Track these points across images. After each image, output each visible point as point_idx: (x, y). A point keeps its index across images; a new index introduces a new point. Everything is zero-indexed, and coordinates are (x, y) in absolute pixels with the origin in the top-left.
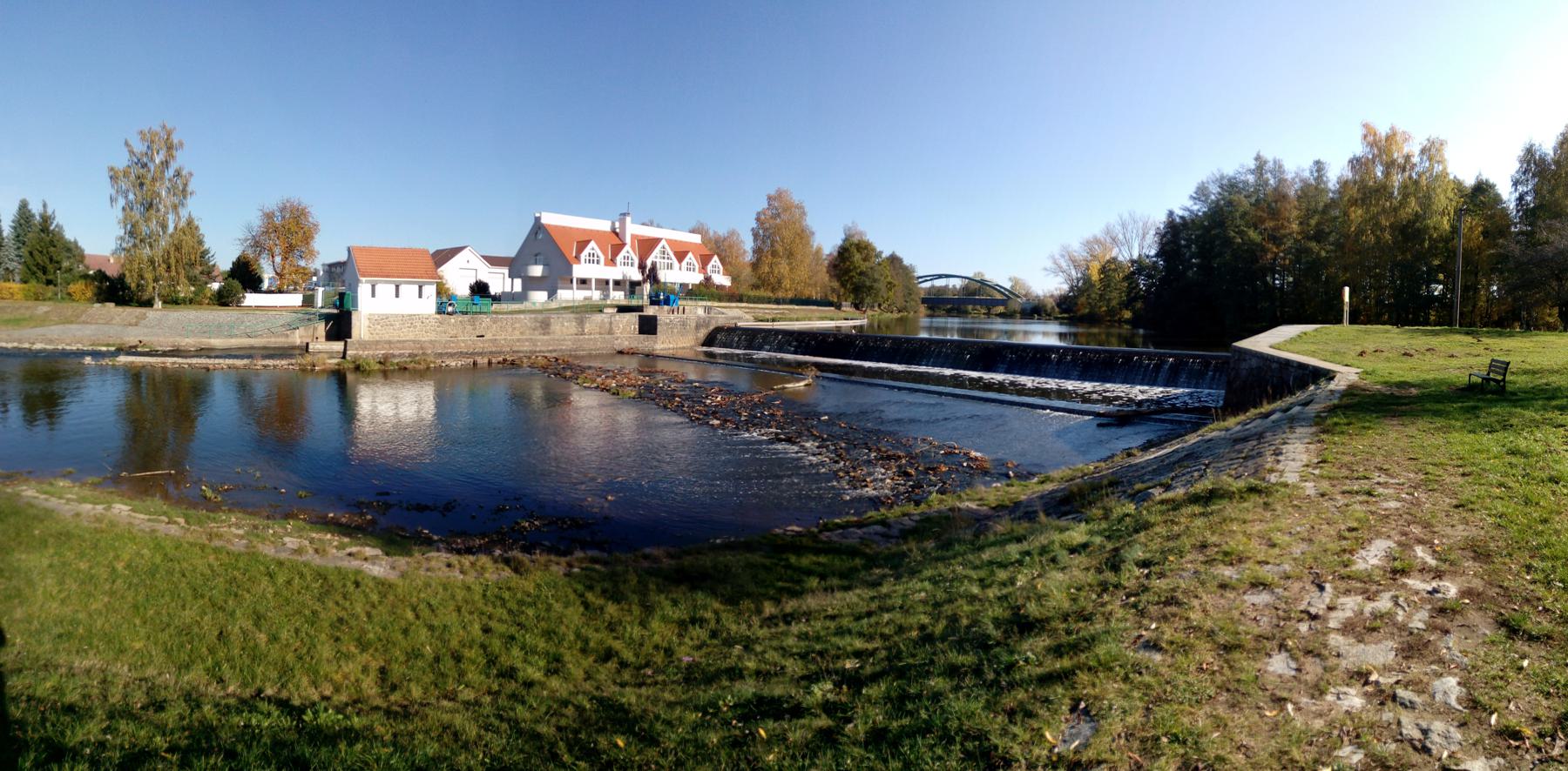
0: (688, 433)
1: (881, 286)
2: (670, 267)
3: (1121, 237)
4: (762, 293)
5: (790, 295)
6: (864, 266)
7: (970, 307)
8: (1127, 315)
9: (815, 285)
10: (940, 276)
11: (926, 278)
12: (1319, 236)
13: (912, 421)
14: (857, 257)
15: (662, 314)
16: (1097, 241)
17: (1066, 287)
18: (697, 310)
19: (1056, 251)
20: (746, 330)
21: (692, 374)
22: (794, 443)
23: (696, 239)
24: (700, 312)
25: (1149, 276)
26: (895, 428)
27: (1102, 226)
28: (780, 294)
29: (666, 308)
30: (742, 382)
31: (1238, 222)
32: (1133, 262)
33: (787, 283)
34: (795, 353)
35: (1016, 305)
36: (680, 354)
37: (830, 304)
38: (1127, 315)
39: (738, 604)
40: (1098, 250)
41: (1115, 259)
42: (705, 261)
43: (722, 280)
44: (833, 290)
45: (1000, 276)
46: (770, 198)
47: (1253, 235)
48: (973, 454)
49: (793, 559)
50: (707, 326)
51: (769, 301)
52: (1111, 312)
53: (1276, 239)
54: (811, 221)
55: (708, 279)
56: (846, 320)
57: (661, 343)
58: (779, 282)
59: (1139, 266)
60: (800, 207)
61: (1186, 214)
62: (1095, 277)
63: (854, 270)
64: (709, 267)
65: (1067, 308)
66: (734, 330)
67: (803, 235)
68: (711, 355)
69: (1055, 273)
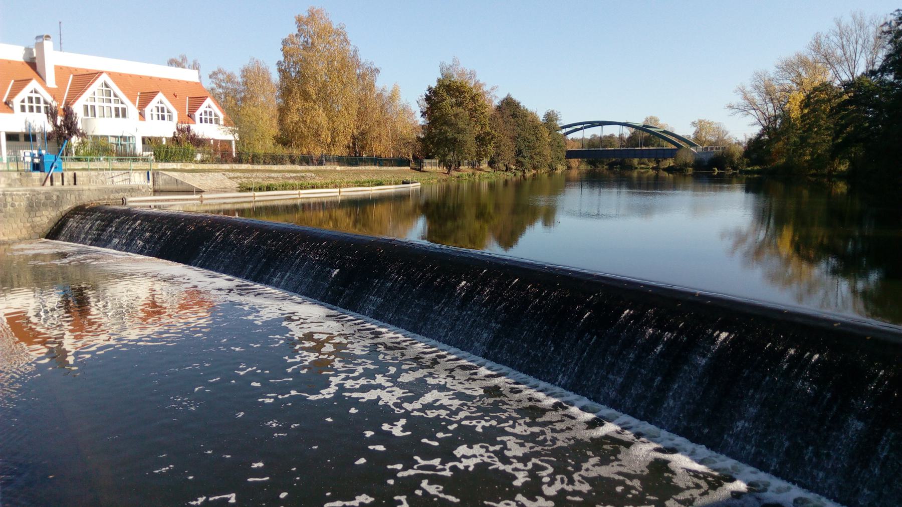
7: (636, 161)
10: (593, 124)
17: (756, 130)
35: (688, 155)
43: (213, 130)
46: (299, 20)
52: (818, 161)
62: (795, 114)
69: (745, 111)
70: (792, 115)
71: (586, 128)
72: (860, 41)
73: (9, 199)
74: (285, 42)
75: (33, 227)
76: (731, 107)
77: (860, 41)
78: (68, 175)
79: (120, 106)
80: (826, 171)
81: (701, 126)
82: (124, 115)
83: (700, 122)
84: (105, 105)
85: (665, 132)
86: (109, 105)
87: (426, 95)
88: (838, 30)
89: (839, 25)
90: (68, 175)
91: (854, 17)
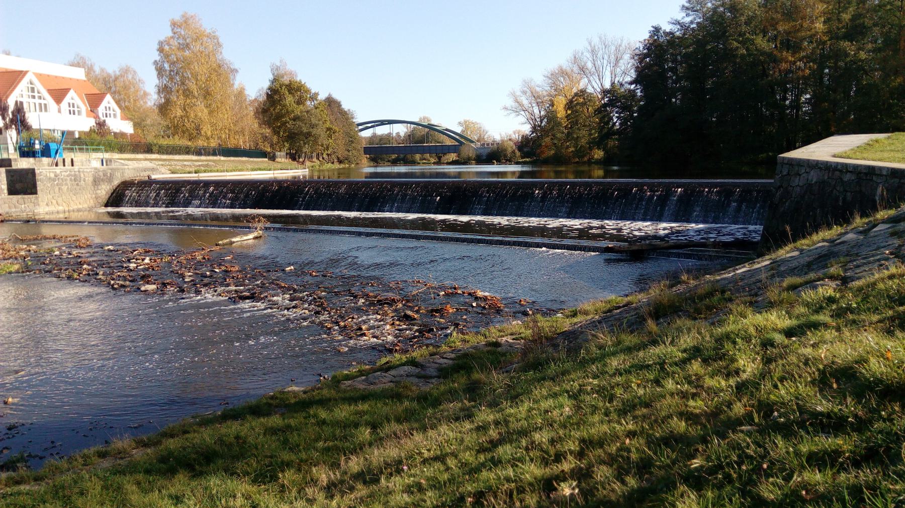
0: (92, 309)
1: (320, 131)
2: (44, 108)
3: (590, 65)
4: (178, 141)
5: (214, 144)
6: (298, 110)
7: (418, 157)
8: (599, 154)
9: (242, 132)
10: (382, 123)
11: (367, 125)
12: (855, 32)
13: (392, 265)
14: (289, 100)
15: (42, 167)
16: (563, 72)
17: (526, 129)
18: (90, 162)
19: (517, 88)
20: (164, 184)
21: (94, 235)
22: (259, 299)
23: (79, 74)
24: (96, 164)
25: (624, 108)
26: (377, 273)
27: (569, 55)
28: (201, 143)
29: (45, 160)
30: (162, 238)
31: (744, 28)
32: (605, 92)
33: (207, 129)
34: (232, 206)
35: (469, 151)
36: (74, 217)
37: (264, 155)
38: (599, 154)
39: (274, 478)
40: (563, 82)
41: (583, 92)
42: (94, 101)
43: (120, 125)
44: (265, 138)
45: (449, 120)
46: (174, 24)
47: (761, 42)
48: (480, 294)
49: (323, 414)
50: (110, 180)
51: (187, 151)
52: (580, 152)
53: (790, 44)
54: (230, 54)
55: (101, 125)
56: (283, 171)
57: (44, 205)
58: (198, 129)
59: (614, 97)
60: (213, 37)
61: (675, 28)
62: (561, 113)
63: (285, 115)
64: (101, 110)
65: (528, 148)
66: (148, 183)
67: (221, 73)
68: (119, 215)
70: (559, 115)
71: (377, 125)
72: (606, 57)
73: (82, 175)
74: (161, 43)
75: (96, 198)
76: (506, 108)
77: (606, 57)
78: (68, 162)
79: (42, 102)
80: (586, 159)
81: (466, 124)
82: (46, 110)
83: (465, 122)
84: (32, 100)
85: (447, 130)
86: (34, 100)
87: (267, 94)
88: (589, 48)
89: (590, 44)
90: (68, 162)
91: (600, 38)
